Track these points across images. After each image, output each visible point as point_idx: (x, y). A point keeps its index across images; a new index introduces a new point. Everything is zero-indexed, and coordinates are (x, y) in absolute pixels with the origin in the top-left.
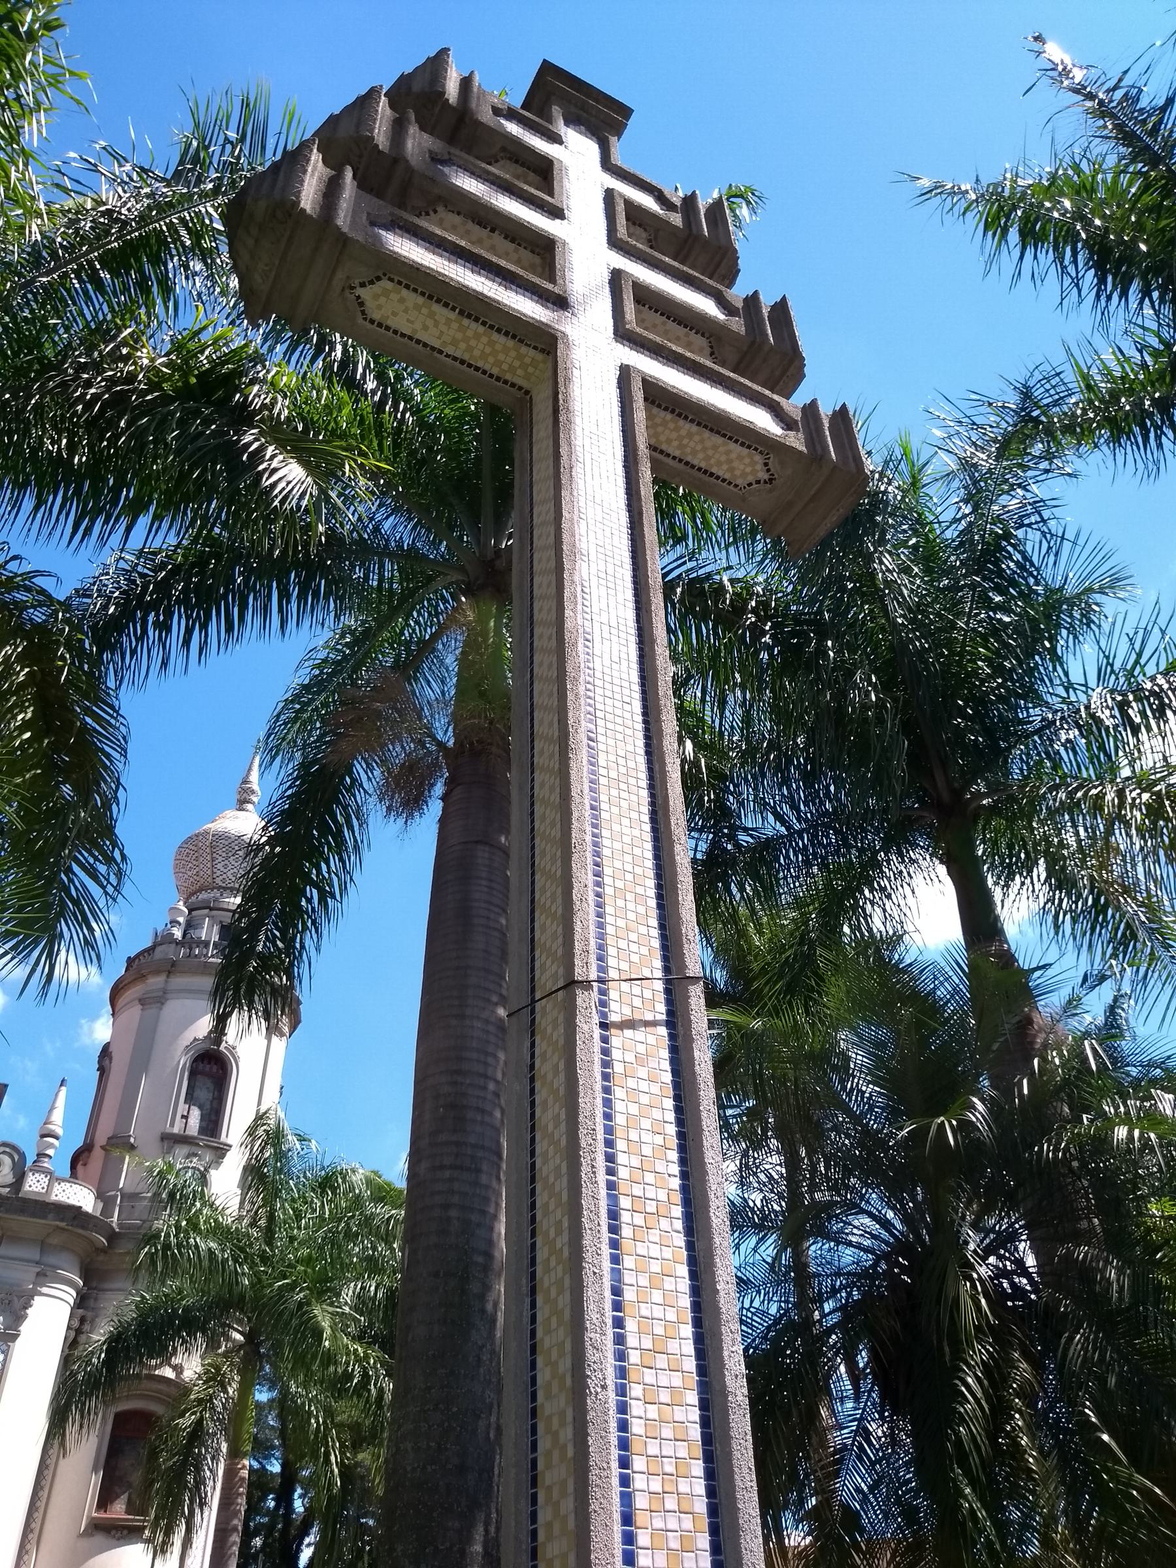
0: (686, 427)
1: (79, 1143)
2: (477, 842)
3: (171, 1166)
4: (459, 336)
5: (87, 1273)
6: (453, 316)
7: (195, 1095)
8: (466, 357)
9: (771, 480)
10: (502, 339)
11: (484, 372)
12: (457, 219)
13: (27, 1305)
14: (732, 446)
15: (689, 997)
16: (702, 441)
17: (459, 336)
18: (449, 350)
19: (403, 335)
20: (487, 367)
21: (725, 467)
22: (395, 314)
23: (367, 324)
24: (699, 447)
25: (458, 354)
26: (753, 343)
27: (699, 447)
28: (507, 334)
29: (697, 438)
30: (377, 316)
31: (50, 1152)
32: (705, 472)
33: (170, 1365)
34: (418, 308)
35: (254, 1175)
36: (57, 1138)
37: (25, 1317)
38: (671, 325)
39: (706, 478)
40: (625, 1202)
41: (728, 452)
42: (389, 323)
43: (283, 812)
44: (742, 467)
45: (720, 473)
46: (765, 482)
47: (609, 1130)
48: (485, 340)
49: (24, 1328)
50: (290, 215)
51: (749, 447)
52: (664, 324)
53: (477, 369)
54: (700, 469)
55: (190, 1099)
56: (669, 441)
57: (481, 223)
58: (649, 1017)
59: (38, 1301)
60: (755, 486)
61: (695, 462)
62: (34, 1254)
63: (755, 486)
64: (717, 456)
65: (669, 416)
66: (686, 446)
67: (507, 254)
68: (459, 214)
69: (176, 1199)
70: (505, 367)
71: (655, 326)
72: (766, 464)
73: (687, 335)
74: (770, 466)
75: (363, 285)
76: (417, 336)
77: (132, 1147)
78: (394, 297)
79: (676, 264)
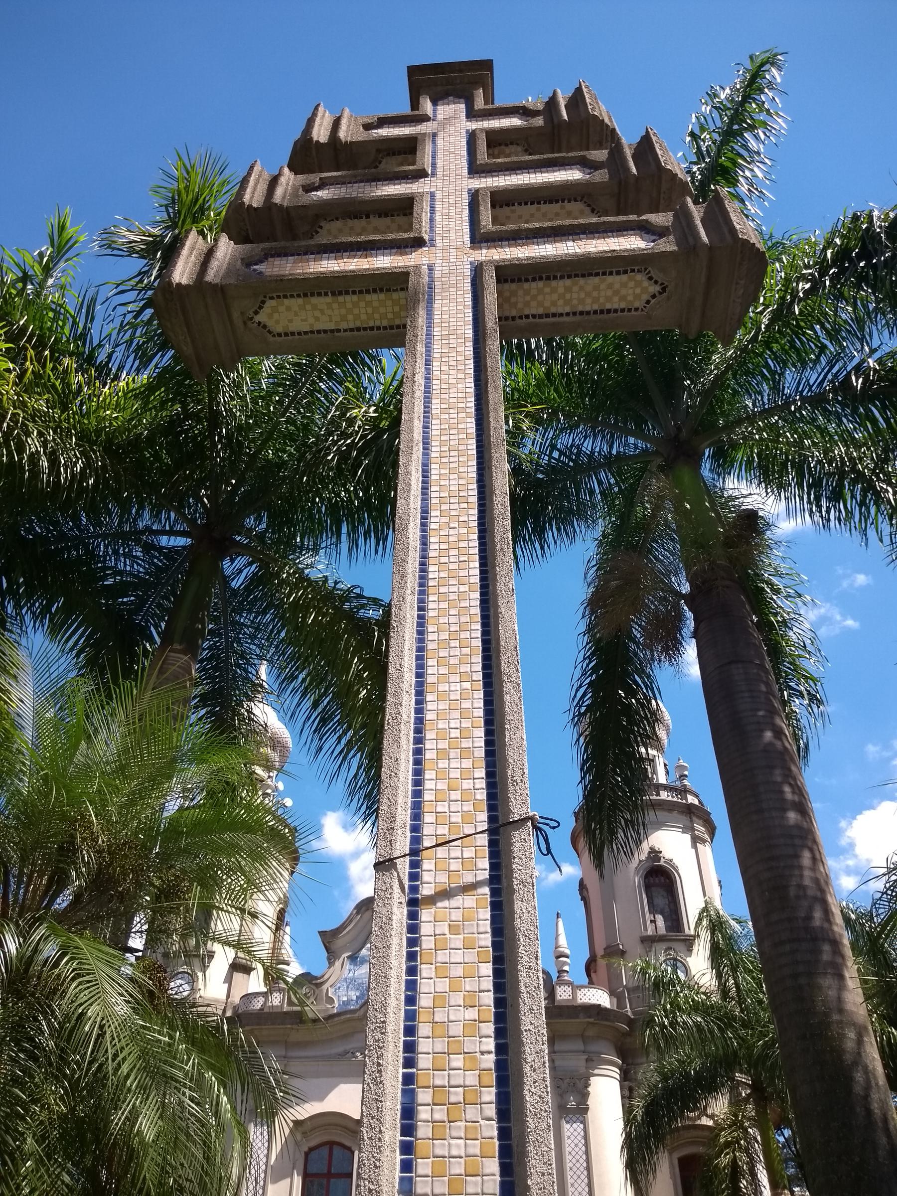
0: (561, 285)
1: (587, 955)
2: (730, 663)
3: (648, 963)
4: (343, 311)
5: (622, 1053)
6: (329, 299)
7: (655, 903)
8: (358, 324)
9: (664, 289)
10: (374, 297)
11: (379, 328)
12: (338, 224)
13: (587, 1085)
14: (610, 279)
15: (512, 844)
16: (582, 288)
17: (343, 311)
18: (344, 326)
19: (306, 333)
20: (378, 323)
21: (616, 299)
22: (291, 321)
23: (277, 339)
24: (582, 295)
25: (351, 326)
26: (620, 183)
27: (582, 295)
28: (375, 291)
29: (575, 289)
30: (279, 329)
31: (566, 968)
32: (602, 312)
33: (707, 1116)
34: (302, 307)
35: (716, 955)
36: (567, 957)
37: (588, 1094)
38: (545, 207)
39: (605, 316)
40: (424, 1096)
41: (610, 286)
42: (291, 329)
43: (590, 684)
44: (631, 291)
45: (616, 306)
46: (660, 293)
47: (411, 1016)
48: (362, 304)
49: (591, 1102)
50: (172, 292)
51: (625, 272)
52: (538, 210)
53: (372, 328)
54: (595, 312)
55: (653, 910)
56: (554, 304)
57: (357, 216)
58: (469, 878)
59: (593, 1080)
60: (653, 301)
61: (588, 308)
62: (579, 1045)
63: (653, 301)
64: (603, 294)
65: (540, 284)
66: (571, 300)
67: (388, 227)
68: (337, 219)
69: (660, 986)
70: (390, 316)
71: (532, 215)
72: (650, 278)
73: (562, 208)
74: (655, 278)
75: (256, 313)
76: (315, 329)
77: (623, 953)
78: (282, 309)
79: (537, 157)
